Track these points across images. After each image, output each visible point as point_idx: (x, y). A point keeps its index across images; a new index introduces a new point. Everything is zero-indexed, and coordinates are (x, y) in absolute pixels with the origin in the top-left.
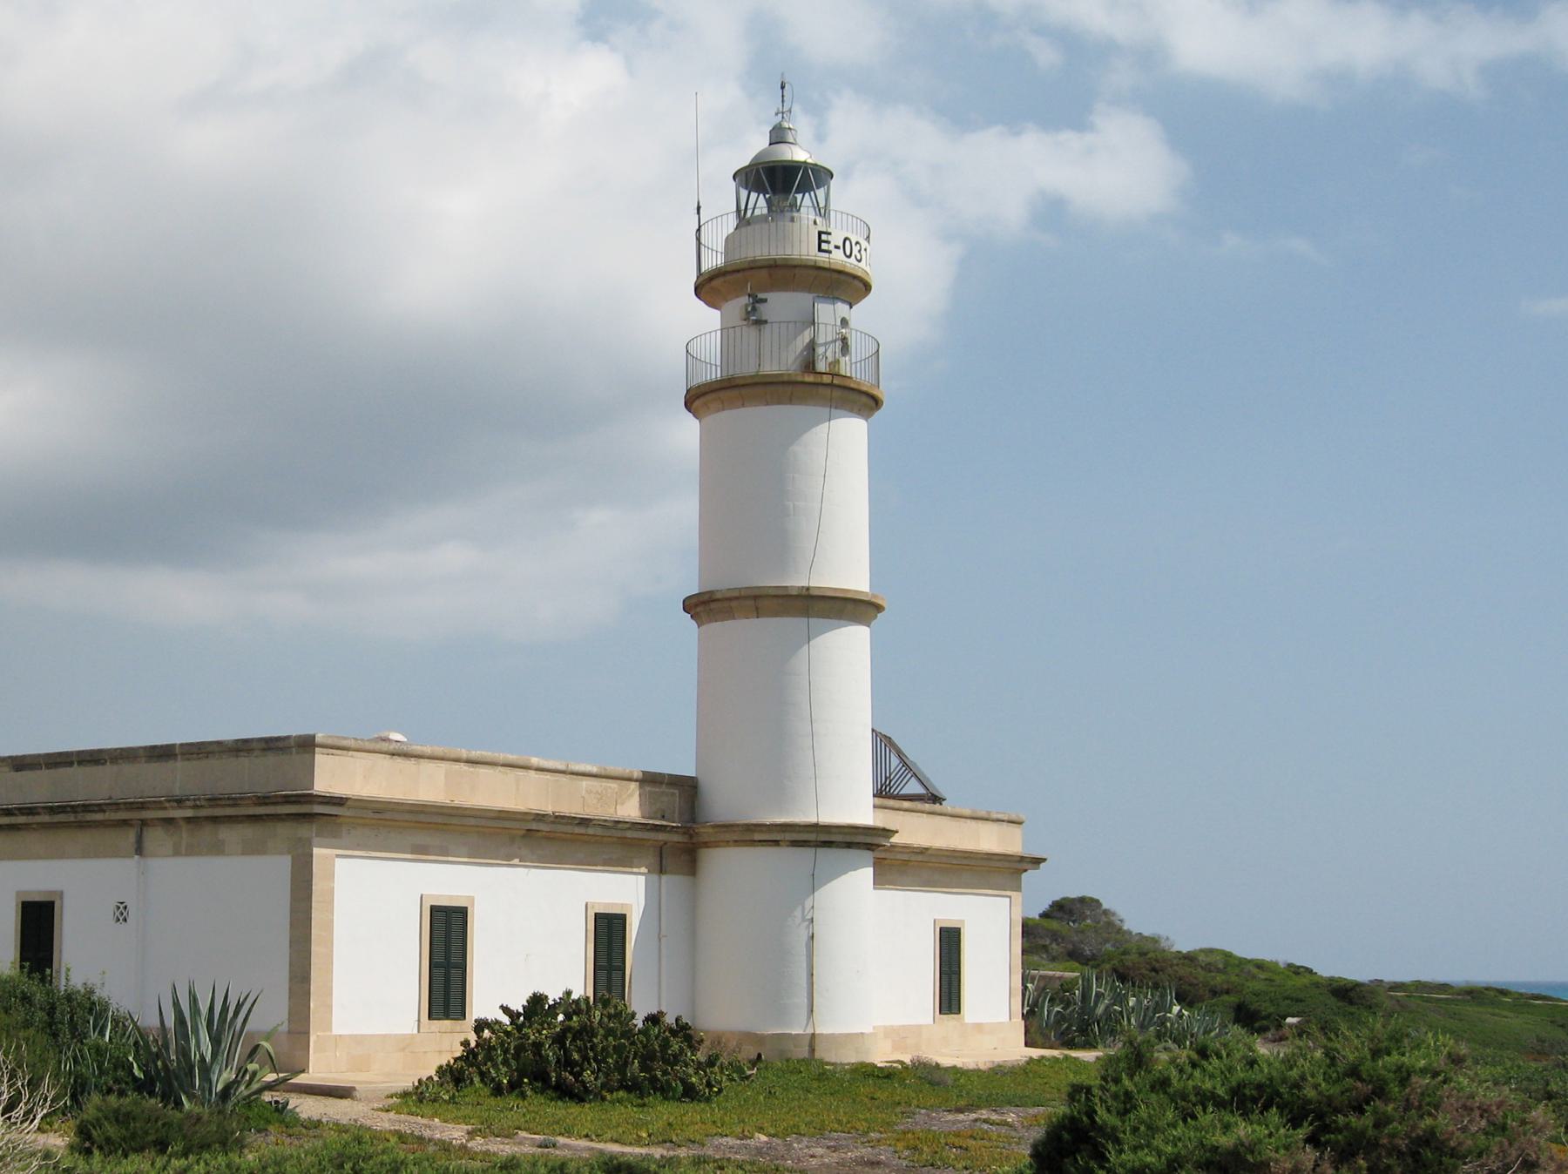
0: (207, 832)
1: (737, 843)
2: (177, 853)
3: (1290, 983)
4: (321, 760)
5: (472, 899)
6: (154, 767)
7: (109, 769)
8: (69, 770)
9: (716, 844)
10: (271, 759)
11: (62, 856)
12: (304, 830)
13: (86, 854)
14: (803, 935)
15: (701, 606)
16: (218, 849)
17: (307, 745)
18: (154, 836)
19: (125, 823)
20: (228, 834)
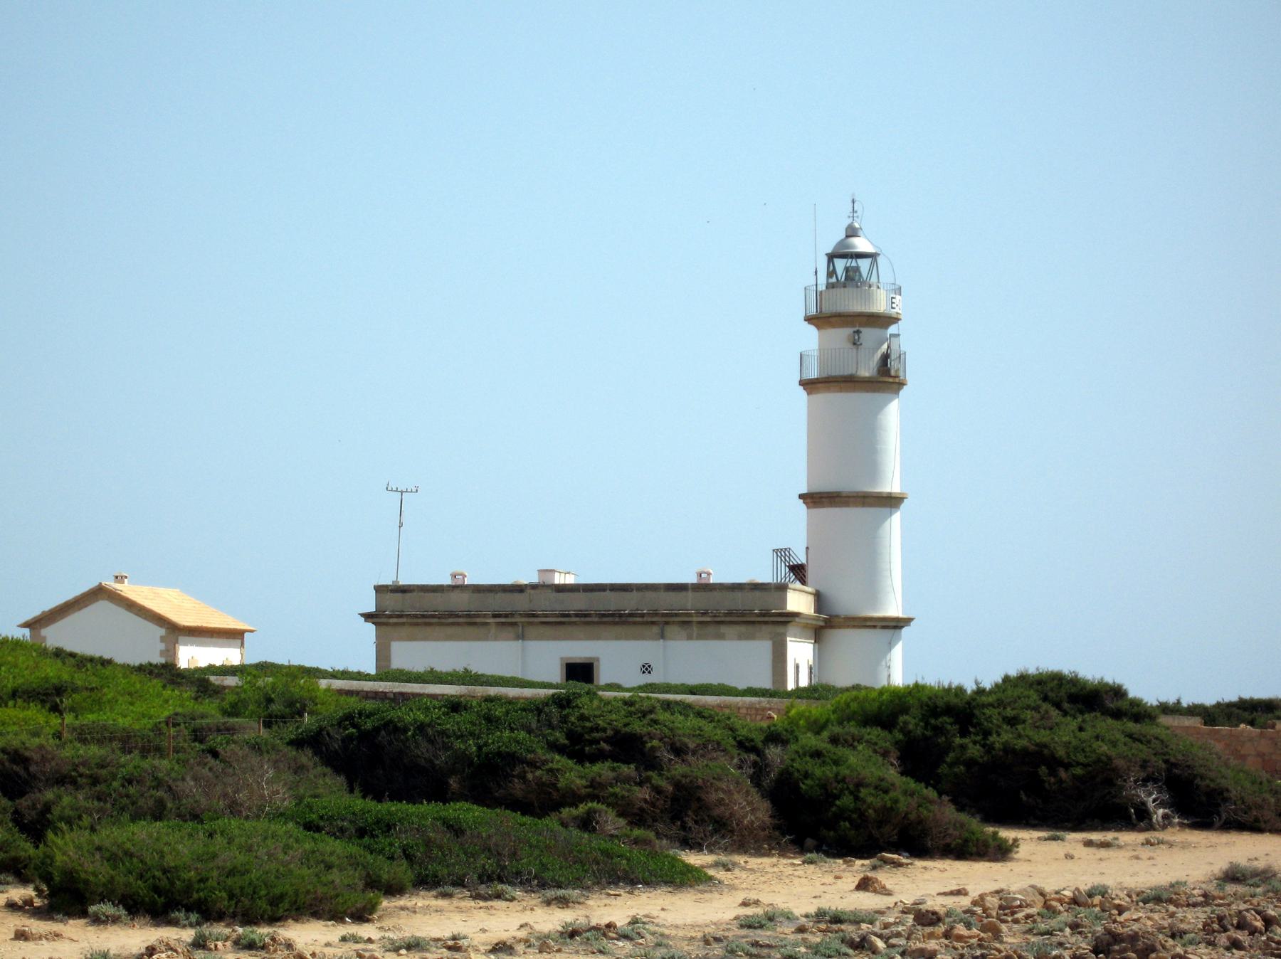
0: (711, 629)
1: (854, 627)
2: (690, 638)
3: (67, 753)
4: (557, 575)
5: (598, 659)
6: (672, 594)
7: (635, 594)
8: (602, 594)
9: (840, 627)
10: (757, 594)
11: (599, 638)
12: (780, 629)
13: (618, 638)
14: (886, 674)
15: (812, 499)
16: (721, 637)
17: (553, 571)
18: (670, 630)
19: (653, 623)
20: (723, 629)
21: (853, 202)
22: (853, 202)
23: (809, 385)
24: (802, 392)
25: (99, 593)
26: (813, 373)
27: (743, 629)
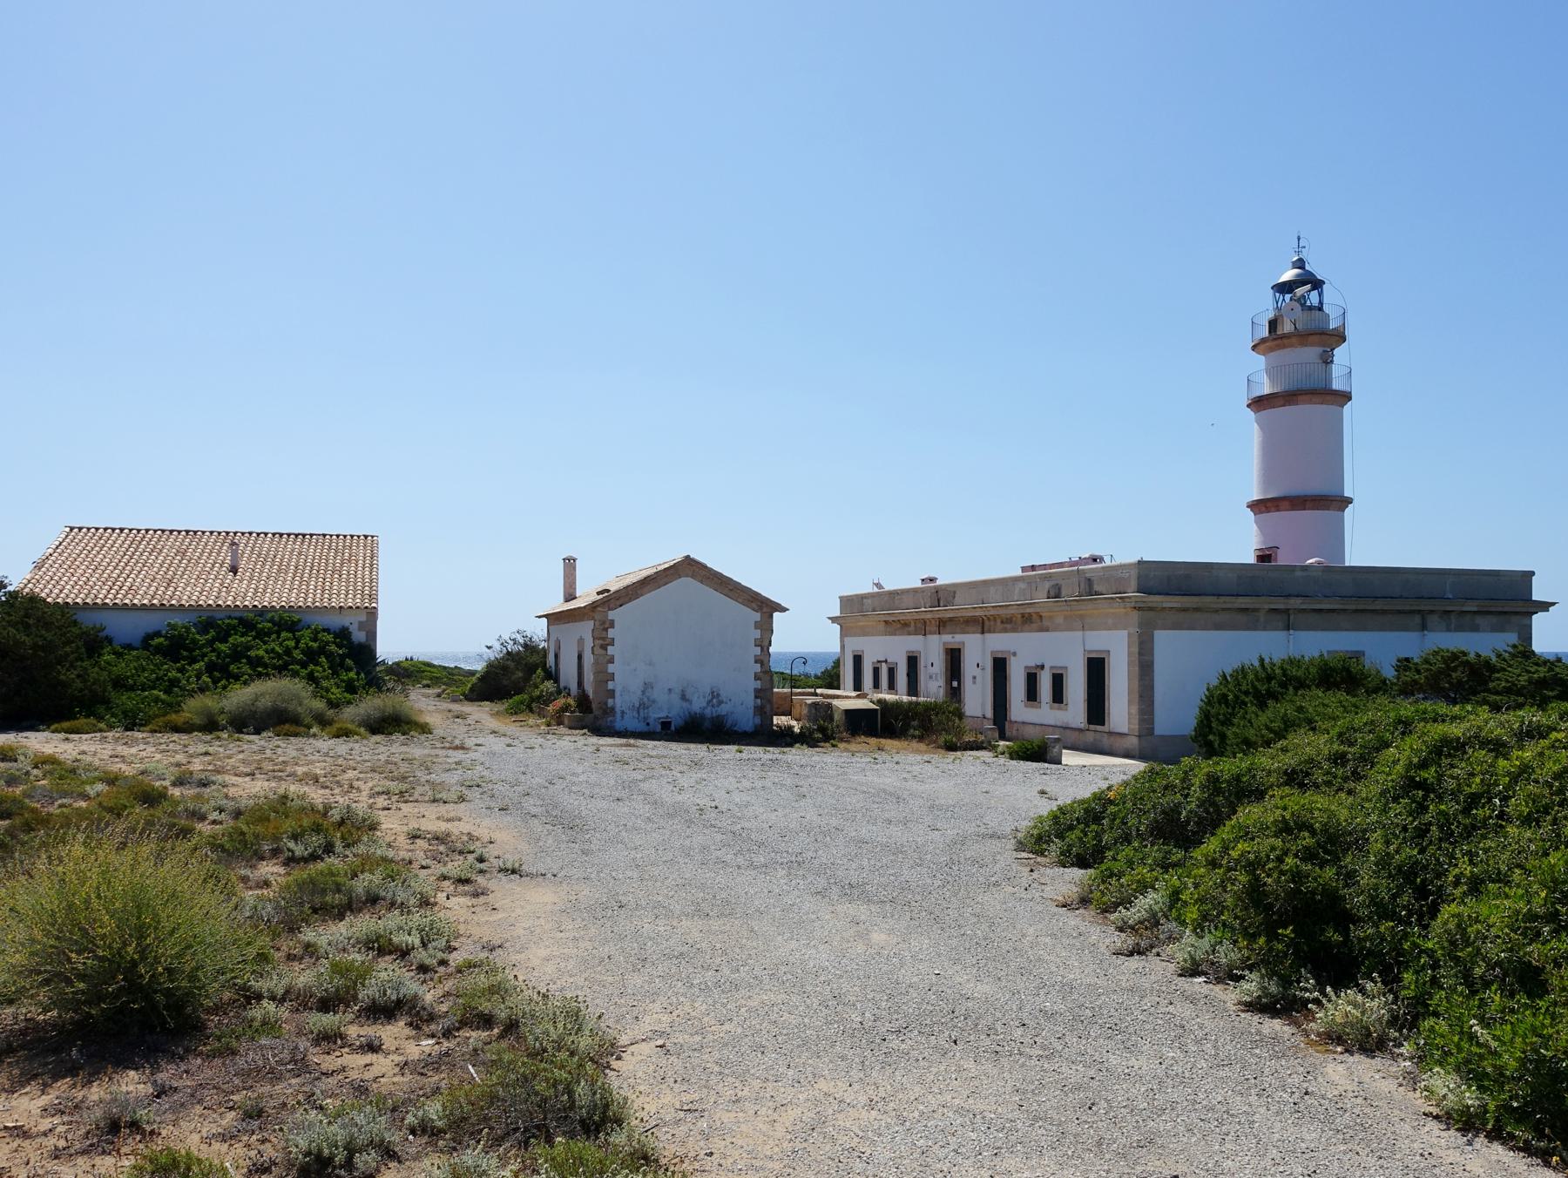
2: (1449, 630)
13: (1382, 629)
20: (1479, 620)
23: (1259, 403)
24: (1250, 414)
25: (689, 567)
27: (1494, 619)
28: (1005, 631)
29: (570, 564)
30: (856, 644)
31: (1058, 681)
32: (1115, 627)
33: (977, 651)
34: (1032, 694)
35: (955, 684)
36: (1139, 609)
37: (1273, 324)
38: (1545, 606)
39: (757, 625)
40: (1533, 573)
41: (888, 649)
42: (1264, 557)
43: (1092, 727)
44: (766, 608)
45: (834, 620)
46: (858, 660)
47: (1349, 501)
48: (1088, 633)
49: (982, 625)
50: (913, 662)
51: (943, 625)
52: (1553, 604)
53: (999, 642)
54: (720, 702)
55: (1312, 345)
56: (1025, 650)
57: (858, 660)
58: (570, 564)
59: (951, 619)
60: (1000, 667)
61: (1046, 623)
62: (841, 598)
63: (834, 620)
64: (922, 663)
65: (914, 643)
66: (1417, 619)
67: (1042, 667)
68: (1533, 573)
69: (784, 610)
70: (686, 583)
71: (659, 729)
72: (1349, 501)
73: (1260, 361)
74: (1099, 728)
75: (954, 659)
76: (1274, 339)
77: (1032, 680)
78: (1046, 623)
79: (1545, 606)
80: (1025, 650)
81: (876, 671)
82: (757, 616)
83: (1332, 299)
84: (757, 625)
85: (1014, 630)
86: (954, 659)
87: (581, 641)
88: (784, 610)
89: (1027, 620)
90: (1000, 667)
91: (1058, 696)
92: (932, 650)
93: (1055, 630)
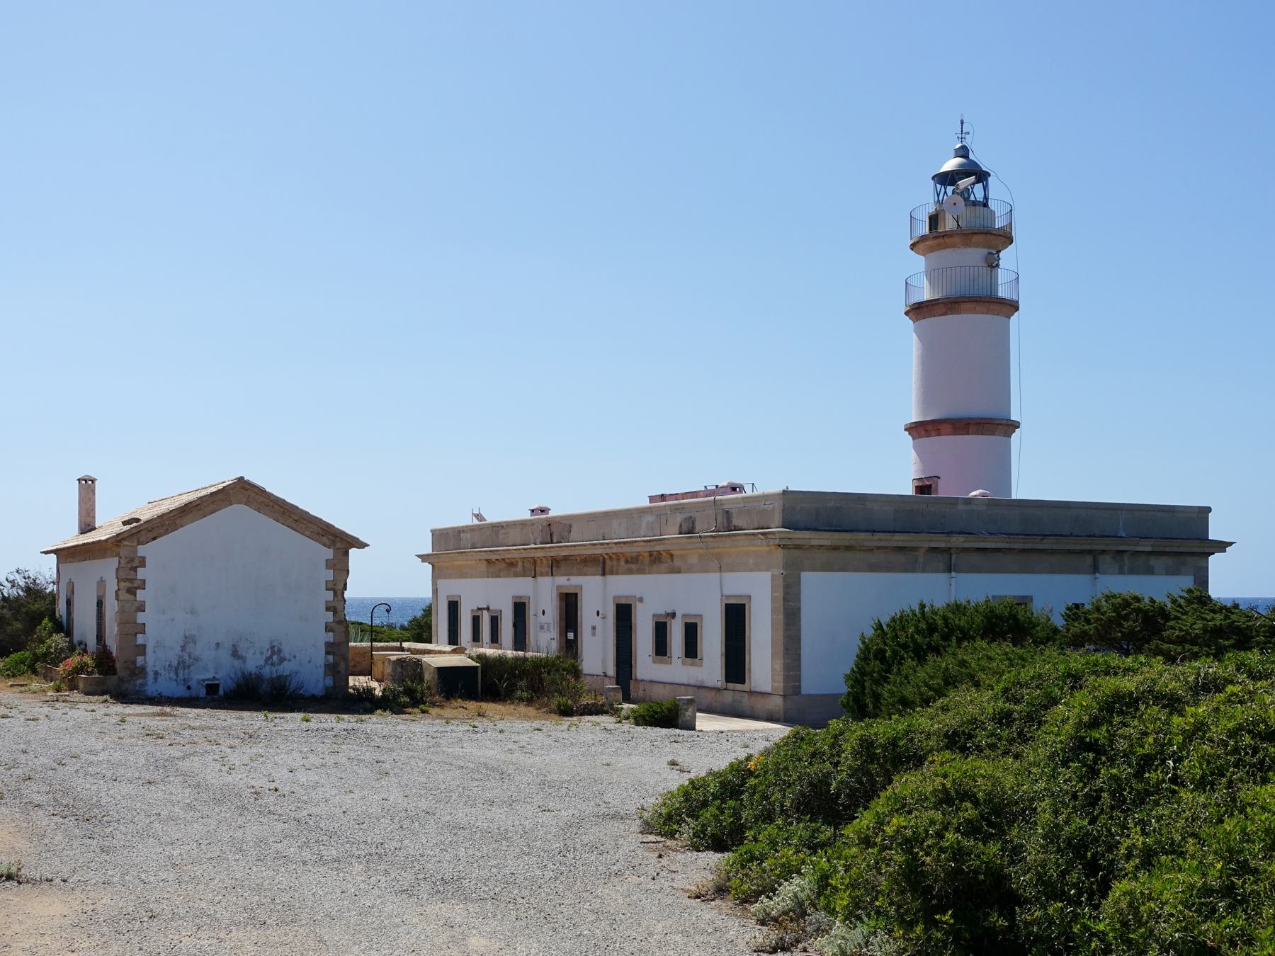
2: (1121, 572)
20: (1154, 561)
21: (962, 123)
22: (962, 123)
23: (918, 311)
24: (908, 322)
25: (243, 492)
26: (926, 295)
28: (630, 572)
29: (87, 486)
30: (452, 587)
31: (691, 632)
32: (757, 568)
33: (597, 597)
34: (661, 648)
35: (571, 636)
36: (784, 547)
37: (934, 220)
38: (1222, 546)
39: (329, 564)
40: (1209, 509)
41: (488, 593)
42: (924, 488)
43: (731, 686)
44: (340, 544)
45: (424, 558)
46: (454, 607)
47: (1016, 425)
48: (609, 578)
49: (602, 565)
50: (520, 609)
51: (556, 565)
52: (1231, 544)
53: (623, 585)
54: (282, 660)
55: (977, 245)
56: (654, 595)
57: (454, 607)
58: (87, 486)
59: (566, 558)
60: (624, 614)
61: (677, 563)
62: (433, 532)
63: (424, 558)
64: (531, 611)
65: (521, 586)
66: (1089, 560)
67: (673, 615)
68: (1209, 509)
69: (362, 545)
70: (238, 512)
71: (203, 693)
72: (1016, 425)
73: (918, 262)
74: (739, 687)
75: (569, 605)
76: (935, 237)
77: (661, 630)
78: (677, 563)
79: (1222, 546)
80: (654, 595)
81: (476, 621)
82: (329, 553)
83: (998, 194)
84: (329, 564)
85: (641, 571)
86: (569, 605)
87: (101, 584)
88: (362, 545)
89: (655, 560)
90: (624, 614)
91: (691, 650)
92: (543, 595)
93: (690, 570)
